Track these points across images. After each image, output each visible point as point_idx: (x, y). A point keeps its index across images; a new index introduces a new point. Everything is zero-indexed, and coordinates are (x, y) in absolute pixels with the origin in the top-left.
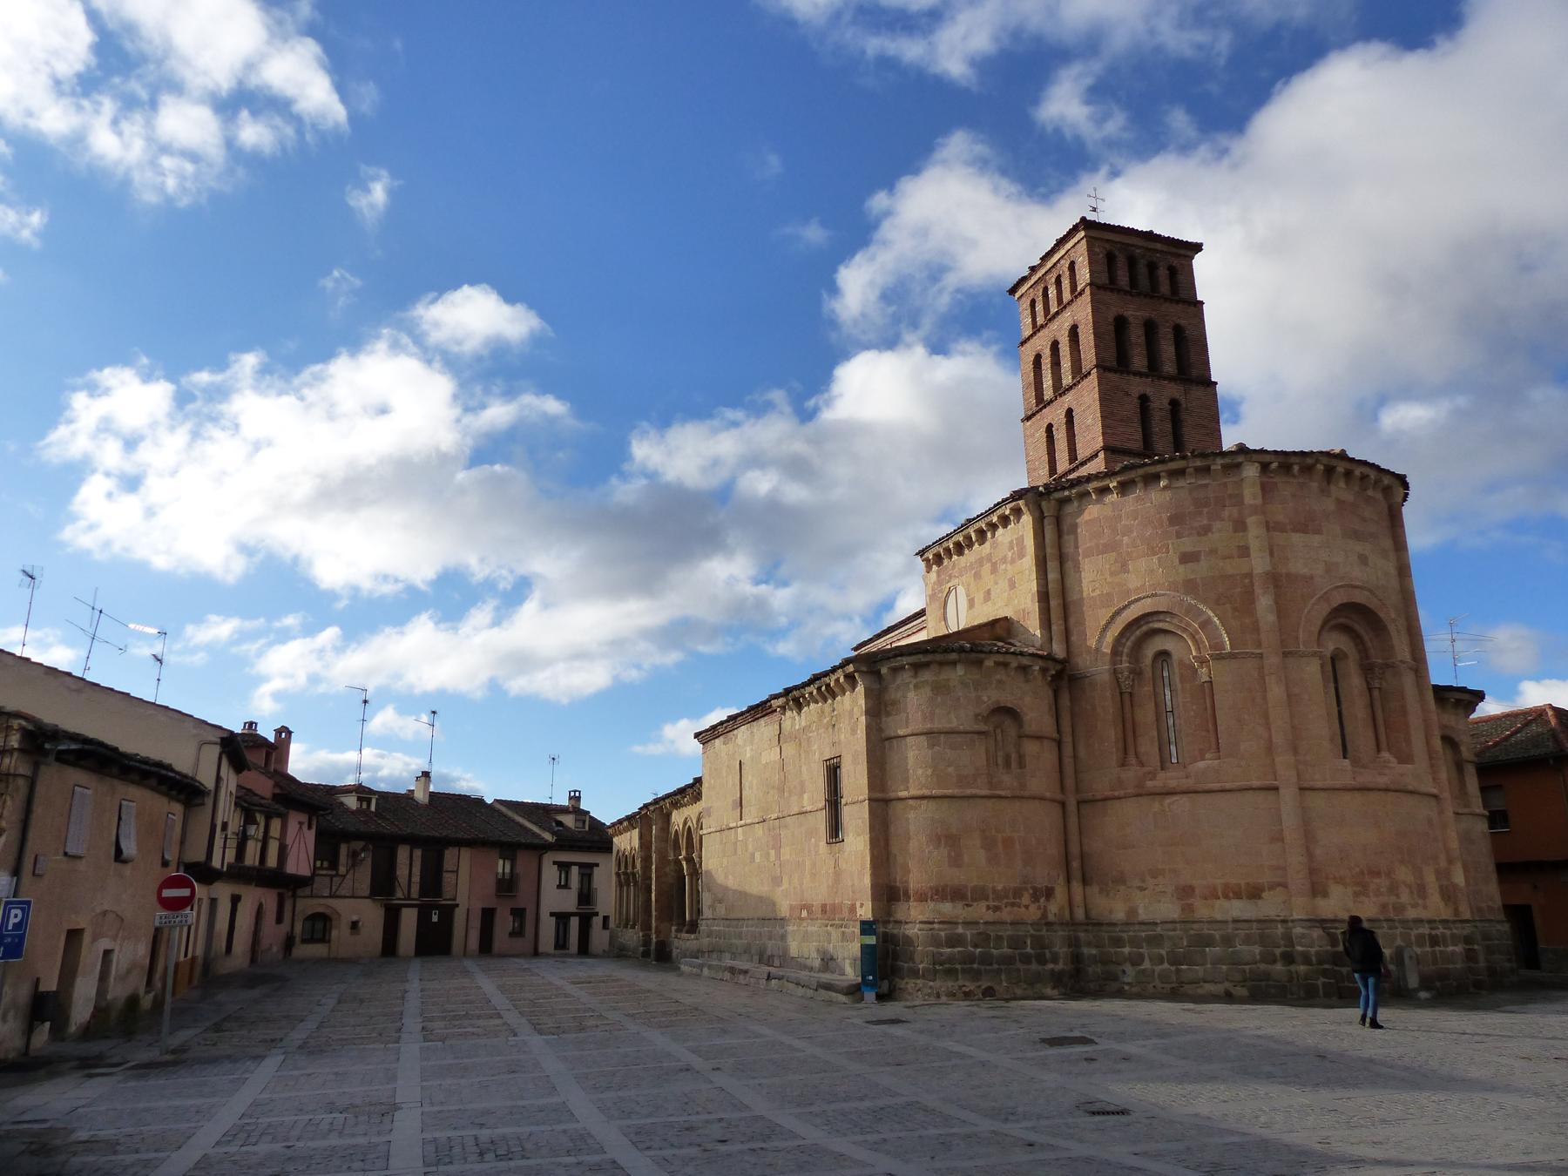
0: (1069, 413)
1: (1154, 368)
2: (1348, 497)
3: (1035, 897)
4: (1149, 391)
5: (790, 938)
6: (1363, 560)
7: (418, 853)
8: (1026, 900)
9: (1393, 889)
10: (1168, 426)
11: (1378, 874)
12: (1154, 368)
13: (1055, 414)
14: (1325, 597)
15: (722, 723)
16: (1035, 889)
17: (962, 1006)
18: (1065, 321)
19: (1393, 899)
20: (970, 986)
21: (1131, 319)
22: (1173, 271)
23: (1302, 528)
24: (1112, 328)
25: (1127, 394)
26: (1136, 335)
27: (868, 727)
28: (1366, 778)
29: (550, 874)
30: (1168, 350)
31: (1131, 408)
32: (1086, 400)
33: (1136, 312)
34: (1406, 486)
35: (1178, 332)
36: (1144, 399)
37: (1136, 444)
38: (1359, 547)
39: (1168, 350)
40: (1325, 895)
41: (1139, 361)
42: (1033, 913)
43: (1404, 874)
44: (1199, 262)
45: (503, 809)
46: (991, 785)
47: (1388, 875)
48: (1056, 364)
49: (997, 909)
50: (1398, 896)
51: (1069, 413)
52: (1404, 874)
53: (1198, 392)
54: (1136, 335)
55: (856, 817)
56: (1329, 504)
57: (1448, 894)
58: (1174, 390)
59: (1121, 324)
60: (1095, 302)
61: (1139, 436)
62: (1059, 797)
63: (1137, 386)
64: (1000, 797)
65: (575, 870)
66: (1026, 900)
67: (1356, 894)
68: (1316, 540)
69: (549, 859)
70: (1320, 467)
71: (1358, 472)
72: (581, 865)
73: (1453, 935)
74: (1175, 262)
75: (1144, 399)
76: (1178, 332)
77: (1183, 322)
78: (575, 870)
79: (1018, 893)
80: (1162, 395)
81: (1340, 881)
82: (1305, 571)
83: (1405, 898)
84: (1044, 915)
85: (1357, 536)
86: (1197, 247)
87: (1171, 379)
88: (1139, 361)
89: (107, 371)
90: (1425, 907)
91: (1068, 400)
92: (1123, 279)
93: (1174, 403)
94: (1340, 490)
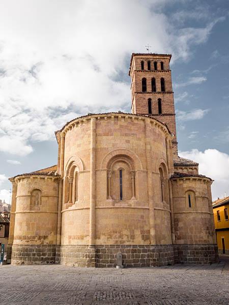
1: (154, 89)
2: (125, 124)
3: (40, 238)
4: (151, 97)
5: (107, 244)
6: (128, 142)
8: (36, 239)
9: (121, 236)
11: (116, 232)
14: (110, 154)
16: (40, 237)
17: (45, 266)
19: (120, 239)
20: (20, 261)
21: (147, 78)
23: (107, 135)
25: (144, 99)
26: (149, 83)
28: (117, 205)
33: (149, 76)
36: (150, 100)
38: (127, 138)
40: (99, 238)
42: (39, 243)
43: (125, 232)
46: (31, 209)
47: (120, 233)
49: (28, 241)
50: (122, 238)
52: (125, 232)
54: (149, 83)
56: (117, 127)
57: (146, 237)
58: (160, 96)
59: (144, 80)
62: (56, 212)
64: (32, 212)
66: (36, 239)
67: (108, 238)
68: (110, 137)
70: (113, 117)
71: (127, 117)
73: (149, 250)
75: (150, 100)
77: (164, 77)
79: (34, 237)
81: (104, 234)
82: (106, 147)
83: (125, 238)
84: (43, 243)
85: (126, 135)
89: (202, 115)
90: (133, 242)
93: (160, 100)
94: (122, 122)
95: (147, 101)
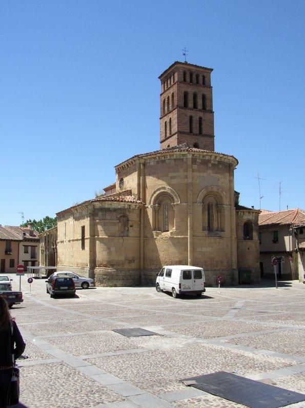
0: (170, 119)
1: (195, 106)
4: (193, 115)
7: (291, 237)
10: (198, 125)
12: (195, 106)
13: (167, 119)
15: (294, 403)
18: (171, 91)
22: (204, 77)
24: (183, 95)
25: (186, 115)
26: (190, 98)
27: (96, 249)
29: (22, 249)
30: (200, 102)
31: (187, 119)
32: (174, 116)
33: (191, 90)
34: (238, 163)
35: (204, 97)
36: (191, 117)
37: (188, 130)
39: (200, 102)
41: (191, 105)
44: (212, 74)
45: (9, 230)
48: (168, 103)
51: (170, 119)
53: (207, 115)
54: (190, 98)
55: (87, 242)
58: (201, 114)
59: (186, 95)
60: (178, 87)
61: (188, 128)
63: (189, 113)
65: (30, 248)
69: (21, 244)
72: (31, 246)
74: (205, 74)
75: (191, 117)
76: (204, 97)
77: (205, 93)
78: (30, 248)
80: (196, 115)
86: (212, 70)
87: (200, 111)
88: (191, 105)
91: (170, 115)
92: (188, 79)
93: (200, 119)
95: (189, 118)
